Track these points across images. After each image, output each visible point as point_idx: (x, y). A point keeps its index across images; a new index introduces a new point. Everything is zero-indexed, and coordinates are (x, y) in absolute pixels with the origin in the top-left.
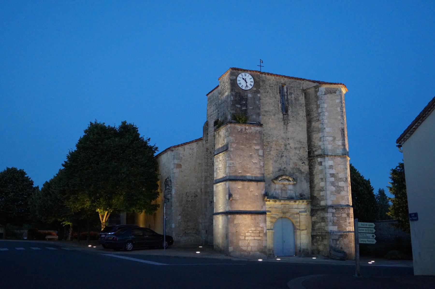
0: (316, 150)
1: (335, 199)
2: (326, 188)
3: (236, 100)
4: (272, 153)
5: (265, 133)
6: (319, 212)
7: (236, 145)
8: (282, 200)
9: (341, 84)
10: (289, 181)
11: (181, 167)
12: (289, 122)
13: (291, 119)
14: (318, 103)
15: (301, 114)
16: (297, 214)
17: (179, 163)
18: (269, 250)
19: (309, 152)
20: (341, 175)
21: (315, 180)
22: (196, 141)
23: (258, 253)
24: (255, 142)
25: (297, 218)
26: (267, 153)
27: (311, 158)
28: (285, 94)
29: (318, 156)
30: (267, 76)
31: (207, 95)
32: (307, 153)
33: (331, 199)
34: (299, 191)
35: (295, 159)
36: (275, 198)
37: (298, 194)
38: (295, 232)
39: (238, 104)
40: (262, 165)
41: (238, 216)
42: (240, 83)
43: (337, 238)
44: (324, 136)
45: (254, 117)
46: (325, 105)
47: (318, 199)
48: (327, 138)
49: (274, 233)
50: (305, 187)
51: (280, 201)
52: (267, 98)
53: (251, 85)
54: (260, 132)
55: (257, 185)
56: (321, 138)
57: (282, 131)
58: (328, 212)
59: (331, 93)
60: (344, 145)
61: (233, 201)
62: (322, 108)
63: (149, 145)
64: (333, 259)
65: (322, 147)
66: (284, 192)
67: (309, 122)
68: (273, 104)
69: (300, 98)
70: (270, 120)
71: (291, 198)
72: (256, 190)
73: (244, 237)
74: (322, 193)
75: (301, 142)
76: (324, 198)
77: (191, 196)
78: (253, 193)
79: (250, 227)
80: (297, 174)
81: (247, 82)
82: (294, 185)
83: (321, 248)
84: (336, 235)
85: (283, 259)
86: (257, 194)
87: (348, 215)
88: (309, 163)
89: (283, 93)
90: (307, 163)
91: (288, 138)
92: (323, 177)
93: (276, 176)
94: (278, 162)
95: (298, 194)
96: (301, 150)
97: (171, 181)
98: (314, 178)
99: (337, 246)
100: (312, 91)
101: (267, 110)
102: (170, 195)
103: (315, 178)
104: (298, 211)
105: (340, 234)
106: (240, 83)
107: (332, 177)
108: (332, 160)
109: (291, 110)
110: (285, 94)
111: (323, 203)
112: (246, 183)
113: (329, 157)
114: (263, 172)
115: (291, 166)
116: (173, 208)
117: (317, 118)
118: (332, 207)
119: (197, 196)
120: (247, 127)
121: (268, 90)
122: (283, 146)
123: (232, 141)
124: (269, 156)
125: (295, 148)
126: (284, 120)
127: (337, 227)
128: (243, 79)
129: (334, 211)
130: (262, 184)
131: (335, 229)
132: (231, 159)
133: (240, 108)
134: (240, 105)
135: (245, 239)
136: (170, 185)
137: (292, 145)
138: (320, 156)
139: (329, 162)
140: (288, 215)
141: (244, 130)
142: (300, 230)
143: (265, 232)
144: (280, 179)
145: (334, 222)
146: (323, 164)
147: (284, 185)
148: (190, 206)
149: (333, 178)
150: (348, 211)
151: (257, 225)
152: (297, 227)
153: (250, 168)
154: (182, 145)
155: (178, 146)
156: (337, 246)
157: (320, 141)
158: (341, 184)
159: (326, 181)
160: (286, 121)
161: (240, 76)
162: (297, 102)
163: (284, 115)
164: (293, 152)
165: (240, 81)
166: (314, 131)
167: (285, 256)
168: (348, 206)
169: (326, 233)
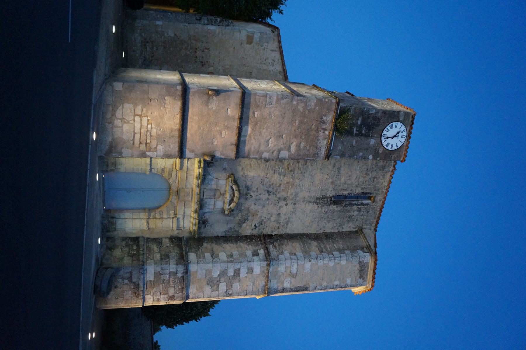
0: (275, 246)
1: (199, 276)
2: (216, 262)
3: (368, 118)
4: (276, 176)
5: (308, 167)
6: (177, 250)
7: (301, 110)
8: (200, 190)
9: (373, 286)
10: (231, 201)
11: (247, 43)
12: (320, 205)
13: (323, 210)
14: (346, 252)
15: (328, 225)
16: (175, 214)
17: (254, 40)
18: (115, 164)
19: (272, 235)
20: (236, 286)
21: (229, 244)
22: (285, 71)
23: (110, 139)
24: (302, 145)
25: (168, 214)
26: (277, 167)
27: (262, 238)
28: (360, 202)
29: (267, 250)
30: (390, 174)
31: (347, 92)
32: (270, 233)
33: (199, 271)
34: (211, 218)
35: (263, 213)
36: (204, 178)
37: (207, 217)
38: (144, 209)
39: (363, 120)
40: (263, 156)
42: (392, 127)
43: (134, 280)
44: (298, 259)
45: (340, 147)
46: (344, 262)
47: (199, 249)
48: (295, 266)
49: (145, 174)
50: (219, 228)
51: (198, 186)
52: (358, 172)
53: (388, 144)
54: (318, 154)
55: (232, 144)
56: (295, 254)
57: (307, 195)
58: (177, 264)
59: (361, 271)
60: (283, 290)
61: (206, 97)
62: (341, 257)
63: (273, 12)
64: (97, 273)
65: (281, 257)
66: (212, 194)
67: (317, 237)
68: (349, 182)
70: (326, 176)
71: (201, 204)
72: (223, 141)
73: (140, 113)
74: (208, 255)
76: (200, 258)
77: (204, 55)
78: (218, 136)
79: (158, 125)
80: (240, 217)
81: (392, 138)
82: (223, 211)
83: (117, 253)
84: (139, 279)
85: (97, 185)
86: (215, 143)
87: (172, 298)
88: (255, 236)
89: (361, 197)
90: (255, 232)
91: (295, 204)
92: (234, 257)
93: (238, 181)
94: (261, 185)
95: (207, 216)
96: (275, 224)
97: (228, 26)
98: (232, 243)
99: (120, 280)
100: (362, 242)
101: (342, 172)
102: (206, 22)
103: (232, 245)
104: (180, 216)
105: (141, 284)
106: (392, 127)
107: (235, 272)
108: (262, 272)
109: (336, 209)
110: (360, 202)
111: (192, 256)
112: (236, 124)
113: (266, 267)
114: (251, 156)
115: (253, 207)
116: (187, 25)
117: (324, 250)
118: (186, 272)
119: (203, 65)
120: (327, 132)
121: (371, 175)
122: (285, 195)
123: (308, 104)
124: (271, 172)
126: (324, 197)
127: (152, 279)
128: (398, 133)
129: (180, 275)
130: (231, 153)
132: (278, 100)
134: (361, 124)
135: (135, 115)
136: (221, 24)
137: (284, 210)
138: (268, 253)
139: (258, 267)
140: (173, 198)
141: (324, 126)
142: (149, 218)
143: (148, 153)
144: (234, 187)
145: (161, 274)
146: (255, 258)
147: (224, 194)
148: (188, 53)
149: (232, 274)
150: (178, 297)
151: (160, 139)
152: (152, 214)
153: (260, 132)
154: (280, 47)
155: (280, 42)
157: (291, 254)
158: (223, 287)
159: (228, 262)
161: (403, 128)
162: (346, 219)
163: (331, 198)
164: (274, 211)
165: (396, 127)
166: (304, 244)
167: (104, 192)
168: (187, 297)
169: (143, 262)
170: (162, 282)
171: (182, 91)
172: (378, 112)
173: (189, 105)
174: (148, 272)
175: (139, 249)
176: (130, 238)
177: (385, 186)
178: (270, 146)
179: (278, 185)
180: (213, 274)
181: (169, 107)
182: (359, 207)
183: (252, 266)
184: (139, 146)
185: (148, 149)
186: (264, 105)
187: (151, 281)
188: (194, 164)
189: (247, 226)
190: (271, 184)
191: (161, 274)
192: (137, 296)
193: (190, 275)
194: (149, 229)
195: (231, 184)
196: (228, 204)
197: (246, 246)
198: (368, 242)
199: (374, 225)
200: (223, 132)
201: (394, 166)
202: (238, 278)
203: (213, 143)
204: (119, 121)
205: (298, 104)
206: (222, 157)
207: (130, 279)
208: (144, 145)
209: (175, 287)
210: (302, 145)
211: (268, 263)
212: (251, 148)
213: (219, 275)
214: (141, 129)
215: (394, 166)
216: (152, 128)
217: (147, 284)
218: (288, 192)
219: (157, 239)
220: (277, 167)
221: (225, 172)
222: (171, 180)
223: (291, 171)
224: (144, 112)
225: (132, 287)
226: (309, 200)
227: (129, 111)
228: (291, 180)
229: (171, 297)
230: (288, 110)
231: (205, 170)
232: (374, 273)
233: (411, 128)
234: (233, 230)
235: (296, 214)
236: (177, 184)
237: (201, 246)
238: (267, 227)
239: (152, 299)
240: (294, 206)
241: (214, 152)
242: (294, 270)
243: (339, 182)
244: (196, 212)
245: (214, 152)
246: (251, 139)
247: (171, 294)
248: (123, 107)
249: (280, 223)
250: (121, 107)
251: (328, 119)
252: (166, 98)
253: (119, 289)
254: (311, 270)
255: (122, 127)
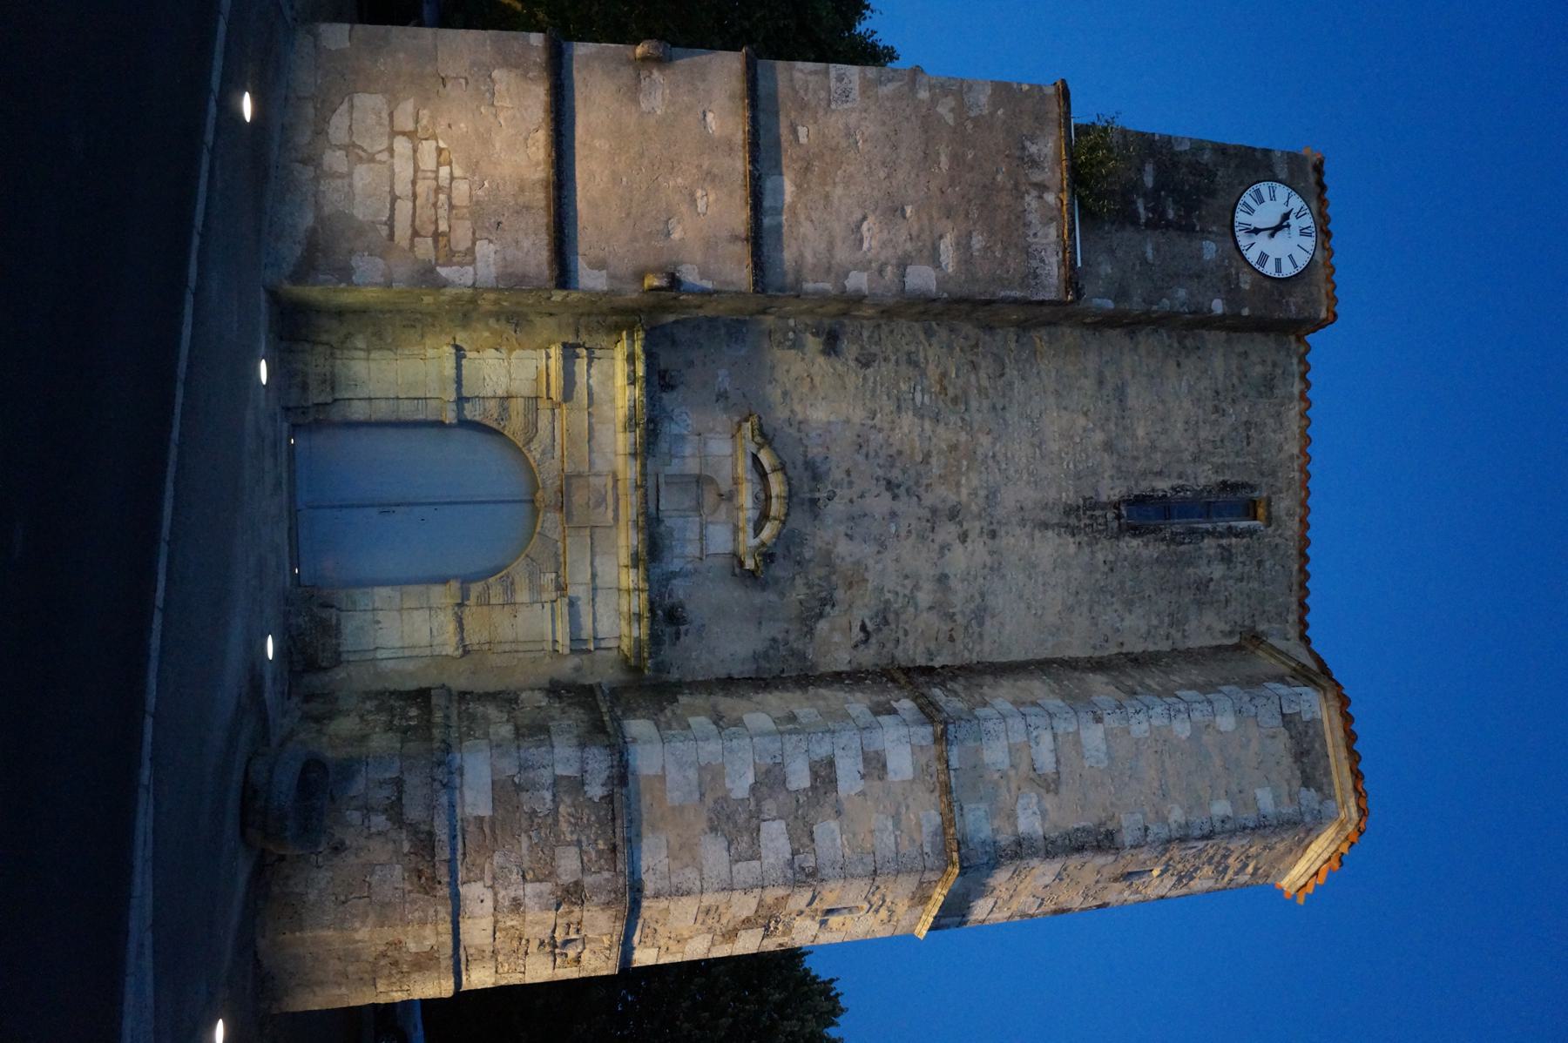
1: (674, 797)
4: (907, 419)
5: (1011, 384)
7: (950, 119)
8: (644, 474)
9: (1363, 812)
13: (1100, 556)
15: (1130, 621)
16: (561, 588)
19: (932, 669)
21: (777, 693)
23: (309, 220)
24: (977, 242)
26: (904, 387)
30: (1295, 409)
32: (921, 661)
33: (673, 773)
36: (651, 429)
39: (1160, 170)
41: (538, 95)
43: (414, 813)
47: (662, 710)
48: (1047, 738)
51: (634, 455)
52: (1187, 404)
53: (1263, 258)
54: (1036, 276)
55: (735, 238)
57: (1029, 495)
58: (582, 746)
68: (1164, 443)
69: (1209, 618)
70: (1082, 421)
73: (410, 127)
75: (981, 624)
78: (684, 208)
79: (473, 167)
80: (799, 592)
81: (1274, 231)
84: (431, 808)
86: (676, 235)
90: (868, 657)
91: (993, 535)
95: (680, 589)
99: (355, 817)
101: (1131, 402)
103: (788, 695)
104: (579, 591)
105: (442, 834)
107: (815, 775)
108: (921, 771)
109: (1145, 553)
110: (1222, 525)
112: (739, 164)
113: (934, 750)
118: (622, 775)
120: (1050, 198)
122: (952, 499)
124: (889, 406)
125: (942, 579)
126: (1092, 505)
127: (485, 810)
128: (1286, 216)
129: (596, 791)
130: (739, 274)
131: (469, 796)
133: (1135, 187)
135: (393, 134)
140: (550, 521)
142: (461, 605)
143: (443, 271)
145: (519, 788)
147: (729, 497)
149: (807, 784)
150: (597, 889)
151: (486, 219)
152: (476, 589)
153: (827, 196)
156: (355, 817)
160: (1082, 517)
161: (1297, 203)
162: (1187, 597)
163: (1116, 506)
170: (525, 824)
171: (545, 48)
172: (1203, 149)
173: (573, 99)
174: (468, 777)
175: (430, 713)
176: (392, 693)
177: (1291, 457)
178: (866, 245)
179: (919, 458)
180: (728, 785)
181: (507, 103)
182: (1224, 542)
183: (877, 746)
184: (412, 245)
185: (442, 253)
186: (823, 104)
187: (480, 819)
188: (613, 377)
189: (832, 630)
190: (893, 451)
191: (519, 788)
192: (428, 885)
193: (638, 793)
194: (466, 652)
195: (752, 448)
196: (750, 531)
197: (841, 694)
198: (1292, 659)
199: (1293, 618)
200: (699, 193)
201: (1303, 377)
202: (832, 797)
203: (668, 234)
204: (338, 153)
205: (934, 101)
206: (708, 285)
207: (395, 811)
208: (430, 240)
209: (579, 843)
210: (977, 242)
211: (940, 728)
212: (802, 255)
213: (753, 789)
214: (414, 183)
215: (1303, 377)
216: (452, 178)
217: (464, 831)
218: (958, 484)
219: (500, 692)
220: (904, 387)
221: (726, 410)
222: (534, 446)
223: (955, 400)
224: (424, 122)
225: (406, 847)
226: (1043, 516)
227: (371, 119)
228: (963, 437)
229: (567, 890)
230: (907, 119)
231: (652, 399)
232: (1354, 757)
233: (1323, 202)
234: (783, 651)
235: (1003, 577)
236: (556, 464)
237: (671, 703)
238: (906, 633)
239: (489, 903)
240: (989, 542)
241: (676, 265)
242: (1046, 762)
243: (1129, 443)
244: (635, 561)
245: (676, 265)
246: (798, 223)
247: (566, 879)
248: (352, 106)
249: (952, 617)
250: (345, 106)
251: (1045, 150)
252: (496, 74)
253: (352, 859)
254: (1110, 756)
255: (350, 174)
